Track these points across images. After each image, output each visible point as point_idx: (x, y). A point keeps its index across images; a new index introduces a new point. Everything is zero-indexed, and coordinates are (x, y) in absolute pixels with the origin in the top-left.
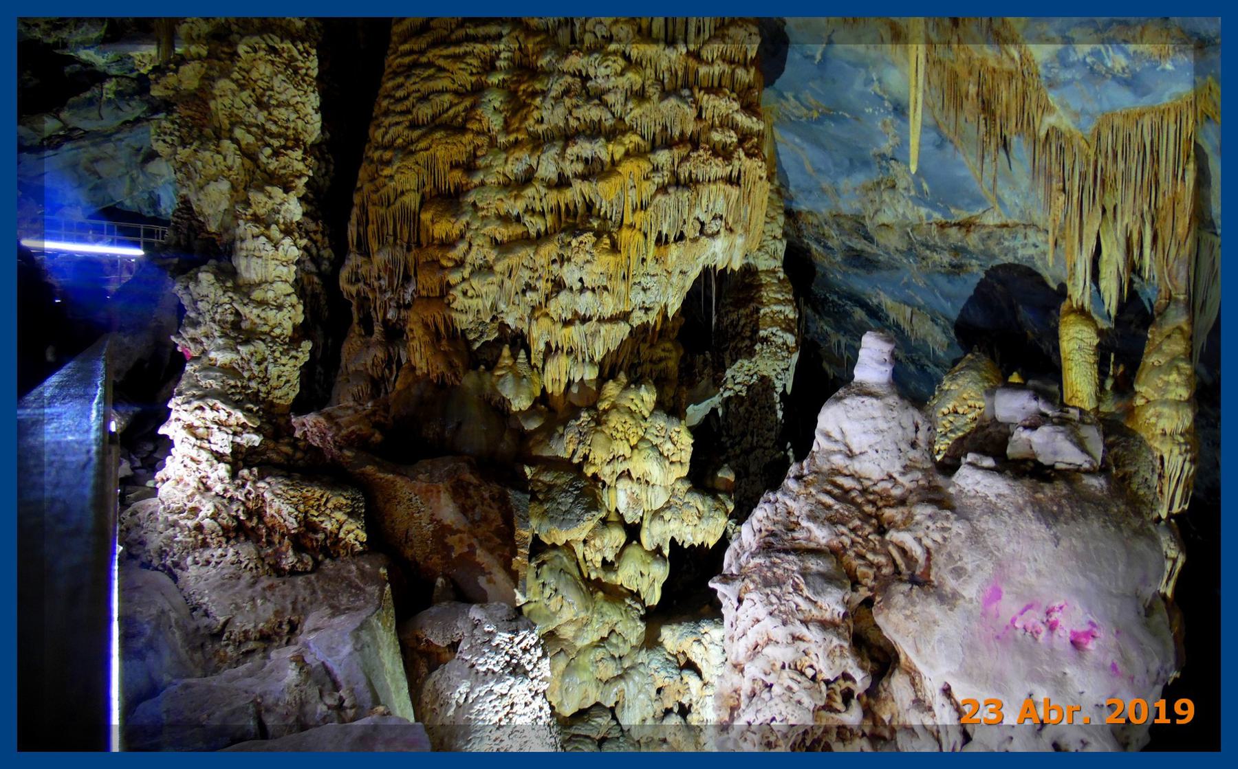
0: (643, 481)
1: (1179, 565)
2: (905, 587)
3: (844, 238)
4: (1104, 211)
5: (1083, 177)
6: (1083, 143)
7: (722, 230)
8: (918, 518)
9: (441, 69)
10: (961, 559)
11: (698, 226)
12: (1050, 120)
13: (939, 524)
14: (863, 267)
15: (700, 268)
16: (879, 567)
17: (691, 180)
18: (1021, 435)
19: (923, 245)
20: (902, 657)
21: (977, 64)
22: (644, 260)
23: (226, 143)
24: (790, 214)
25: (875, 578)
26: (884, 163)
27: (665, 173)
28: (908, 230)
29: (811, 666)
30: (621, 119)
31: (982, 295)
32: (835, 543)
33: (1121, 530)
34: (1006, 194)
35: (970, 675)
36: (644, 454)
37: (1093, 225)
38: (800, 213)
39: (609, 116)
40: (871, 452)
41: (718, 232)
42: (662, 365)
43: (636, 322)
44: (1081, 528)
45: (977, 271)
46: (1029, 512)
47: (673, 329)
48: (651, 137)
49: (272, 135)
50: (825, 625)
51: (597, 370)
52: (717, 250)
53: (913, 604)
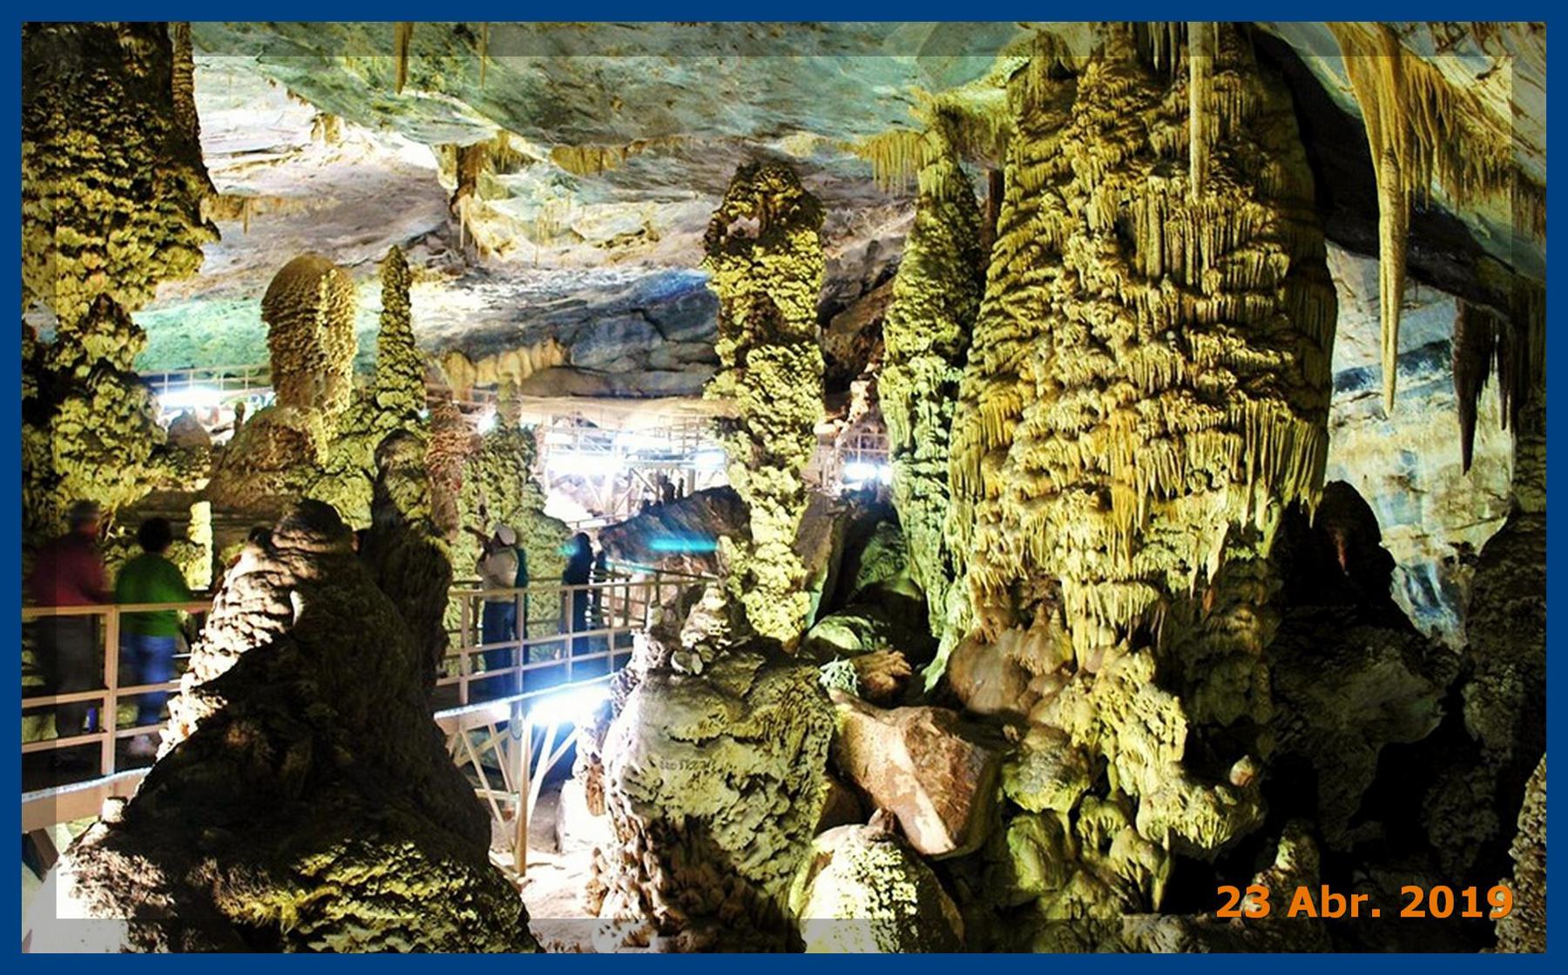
9: (1008, 316)
23: (742, 435)
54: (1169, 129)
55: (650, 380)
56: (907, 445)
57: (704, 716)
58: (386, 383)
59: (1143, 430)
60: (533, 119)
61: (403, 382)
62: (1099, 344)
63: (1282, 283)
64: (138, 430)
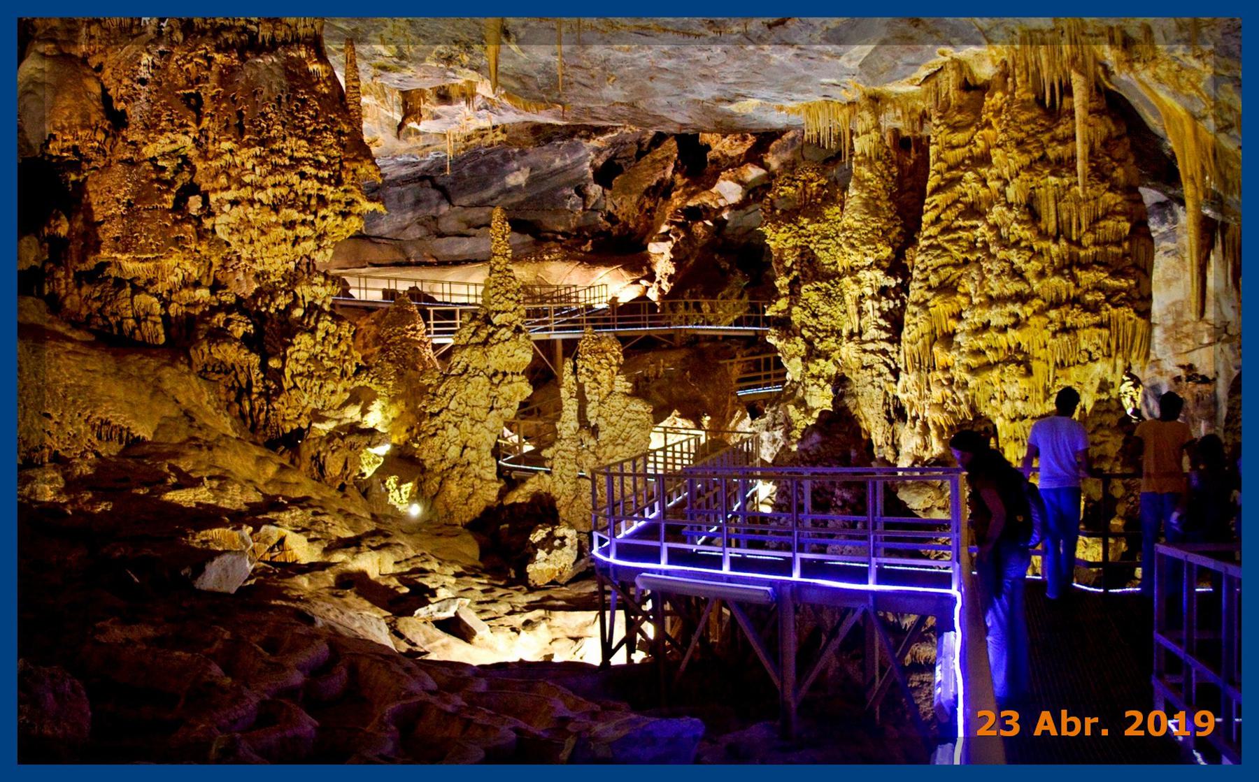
9: (945, 250)
11: (1086, 355)
23: (798, 339)
49: (820, 331)
54: (1060, 148)
55: (448, 248)
56: (856, 330)
57: (926, 497)
58: (501, 307)
59: (1051, 328)
60: (539, 88)
61: (512, 305)
62: (1017, 274)
63: (1126, 239)
64: (346, 354)
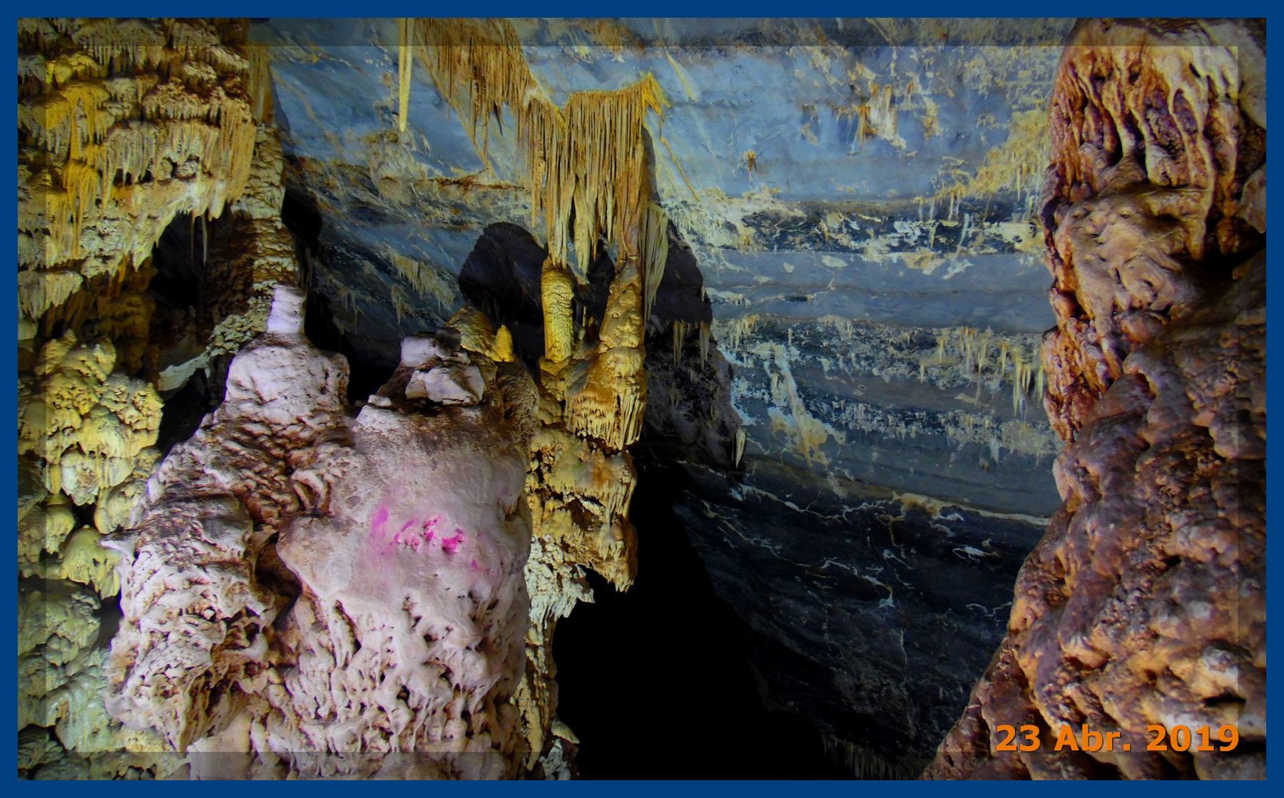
0: (97, 454)
1: (632, 489)
2: (306, 521)
3: (349, 189)
4: (577, 179)
5: (560, 146)
6: (559, 116)
7: (199, 174)
8: (321, 456)
10: (356, 489)
11: (170, 168)
12: (532, 93)
13: (339, 461)
14: (370, 220)
15: (173, 214)
16: (284, 505)
17: (159, 116)
18: (418, 377)
19: (425, 200)
20: (304, 586)
21: (468, 31)
22: (98, 202)
24: (292, 161)
25: (280, 515)
26: (386, 117)
27: (126, 105)
28: (411, 184)
29: (211, 608)
30: (67, 36)
31: (482, 252)
32: (240, 486)
33: (489, 453)
34: (499, 158)
35: (357, 590)
36: (99, 423)
37: (568, 191)
38: (303, 159)
39: (50, 29)
40: (282, 401)
41: (194, 176)
42: (129, 321)
43: (91, 273)
44: (456, 453)
45: (476, 228)
46: (414, 443)
47: (143, 281)
48: (107, 62)
50: (222, 566)
51: (35, 328)
52: (192, 195)
53: (312, 534)
